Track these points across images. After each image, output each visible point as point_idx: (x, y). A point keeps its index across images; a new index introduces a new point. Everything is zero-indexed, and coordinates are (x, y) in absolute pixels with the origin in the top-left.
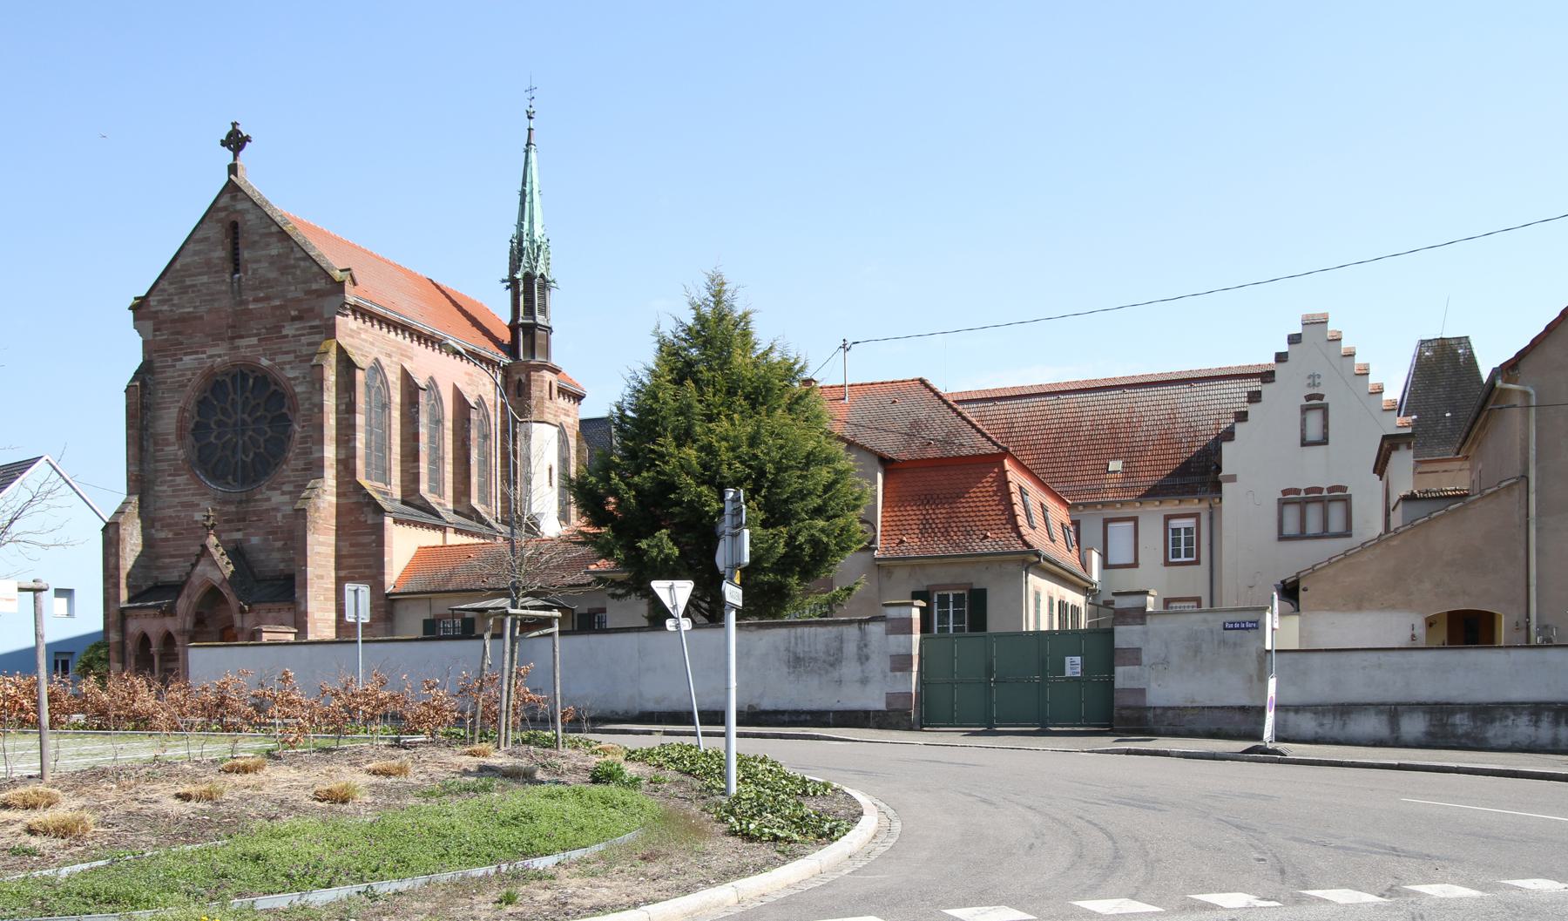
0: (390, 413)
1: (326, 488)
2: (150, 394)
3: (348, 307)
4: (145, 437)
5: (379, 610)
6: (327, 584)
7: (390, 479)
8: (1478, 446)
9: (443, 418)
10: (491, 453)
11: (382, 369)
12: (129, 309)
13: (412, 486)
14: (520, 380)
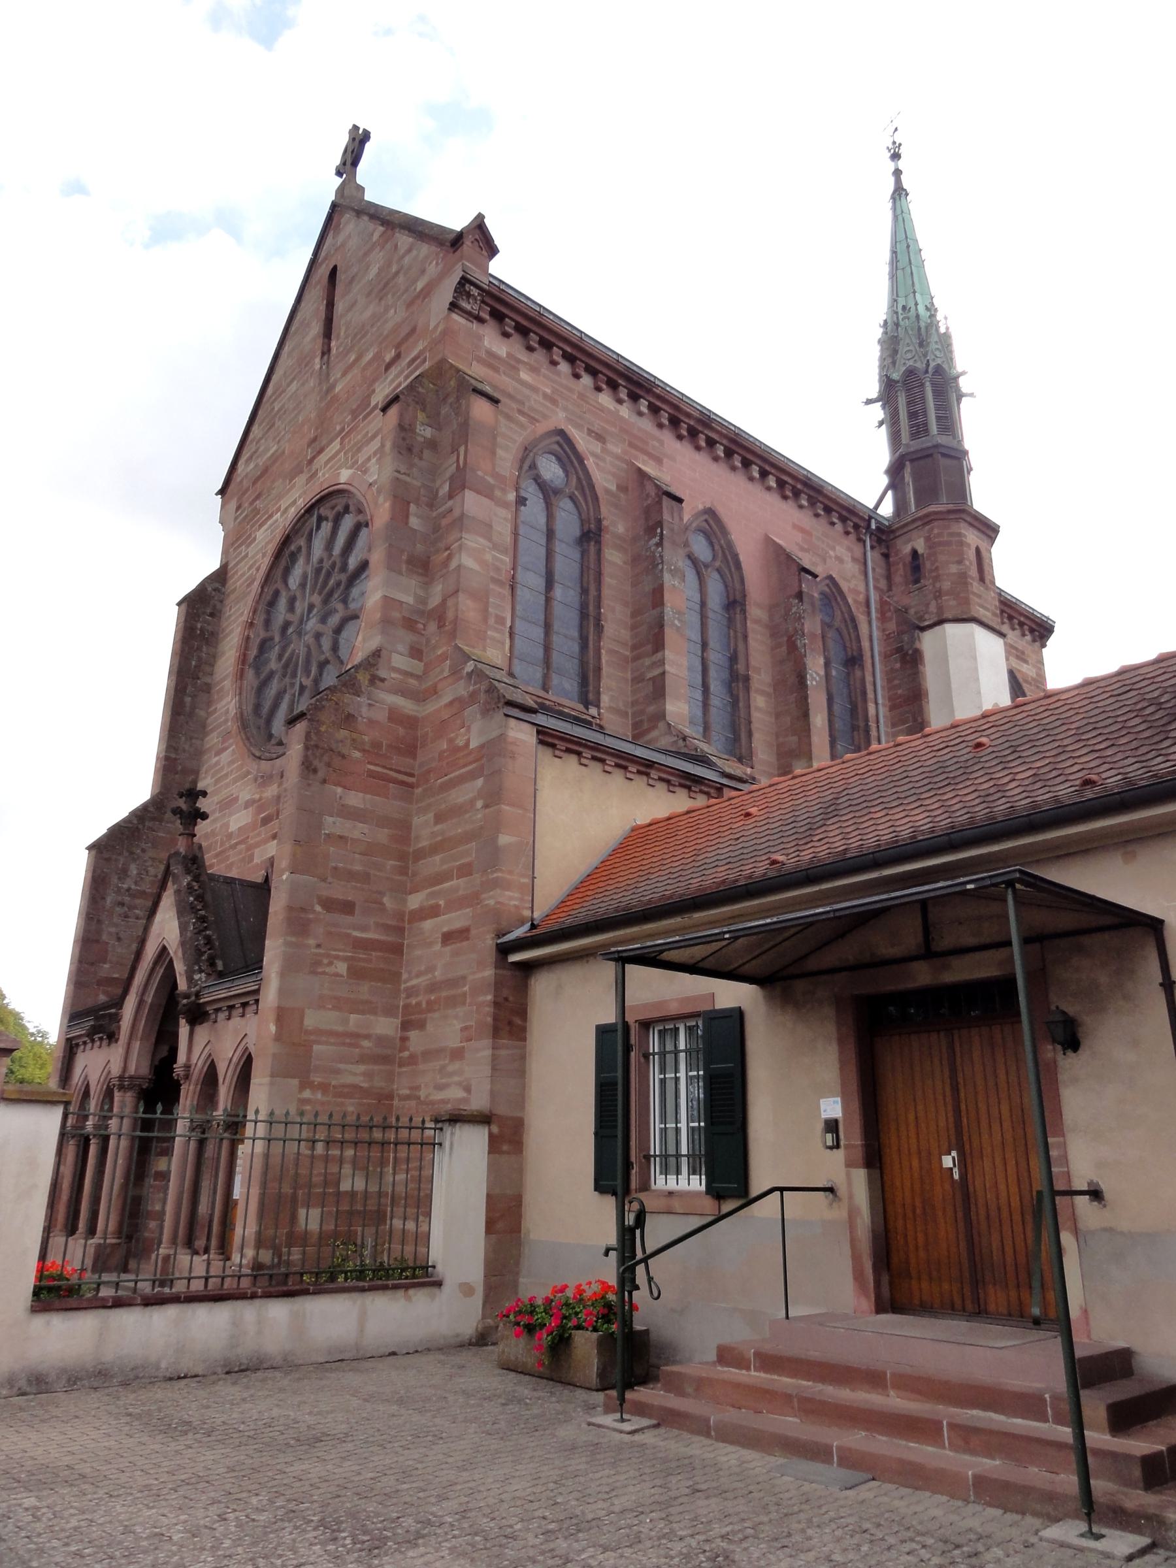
0: (599, 552)
1: (382, 673)
2: (212, 615)
3: (475, 292)
4: (190, 689)
5: (481, 999)
6: (364, 929)
7: (599, 693)
8: (450, 1154)
9: (745, 596)
10: (864, 693)
11: (581, 460)
12: (217, 494)
13: (651, 709)
14: (915, 553)
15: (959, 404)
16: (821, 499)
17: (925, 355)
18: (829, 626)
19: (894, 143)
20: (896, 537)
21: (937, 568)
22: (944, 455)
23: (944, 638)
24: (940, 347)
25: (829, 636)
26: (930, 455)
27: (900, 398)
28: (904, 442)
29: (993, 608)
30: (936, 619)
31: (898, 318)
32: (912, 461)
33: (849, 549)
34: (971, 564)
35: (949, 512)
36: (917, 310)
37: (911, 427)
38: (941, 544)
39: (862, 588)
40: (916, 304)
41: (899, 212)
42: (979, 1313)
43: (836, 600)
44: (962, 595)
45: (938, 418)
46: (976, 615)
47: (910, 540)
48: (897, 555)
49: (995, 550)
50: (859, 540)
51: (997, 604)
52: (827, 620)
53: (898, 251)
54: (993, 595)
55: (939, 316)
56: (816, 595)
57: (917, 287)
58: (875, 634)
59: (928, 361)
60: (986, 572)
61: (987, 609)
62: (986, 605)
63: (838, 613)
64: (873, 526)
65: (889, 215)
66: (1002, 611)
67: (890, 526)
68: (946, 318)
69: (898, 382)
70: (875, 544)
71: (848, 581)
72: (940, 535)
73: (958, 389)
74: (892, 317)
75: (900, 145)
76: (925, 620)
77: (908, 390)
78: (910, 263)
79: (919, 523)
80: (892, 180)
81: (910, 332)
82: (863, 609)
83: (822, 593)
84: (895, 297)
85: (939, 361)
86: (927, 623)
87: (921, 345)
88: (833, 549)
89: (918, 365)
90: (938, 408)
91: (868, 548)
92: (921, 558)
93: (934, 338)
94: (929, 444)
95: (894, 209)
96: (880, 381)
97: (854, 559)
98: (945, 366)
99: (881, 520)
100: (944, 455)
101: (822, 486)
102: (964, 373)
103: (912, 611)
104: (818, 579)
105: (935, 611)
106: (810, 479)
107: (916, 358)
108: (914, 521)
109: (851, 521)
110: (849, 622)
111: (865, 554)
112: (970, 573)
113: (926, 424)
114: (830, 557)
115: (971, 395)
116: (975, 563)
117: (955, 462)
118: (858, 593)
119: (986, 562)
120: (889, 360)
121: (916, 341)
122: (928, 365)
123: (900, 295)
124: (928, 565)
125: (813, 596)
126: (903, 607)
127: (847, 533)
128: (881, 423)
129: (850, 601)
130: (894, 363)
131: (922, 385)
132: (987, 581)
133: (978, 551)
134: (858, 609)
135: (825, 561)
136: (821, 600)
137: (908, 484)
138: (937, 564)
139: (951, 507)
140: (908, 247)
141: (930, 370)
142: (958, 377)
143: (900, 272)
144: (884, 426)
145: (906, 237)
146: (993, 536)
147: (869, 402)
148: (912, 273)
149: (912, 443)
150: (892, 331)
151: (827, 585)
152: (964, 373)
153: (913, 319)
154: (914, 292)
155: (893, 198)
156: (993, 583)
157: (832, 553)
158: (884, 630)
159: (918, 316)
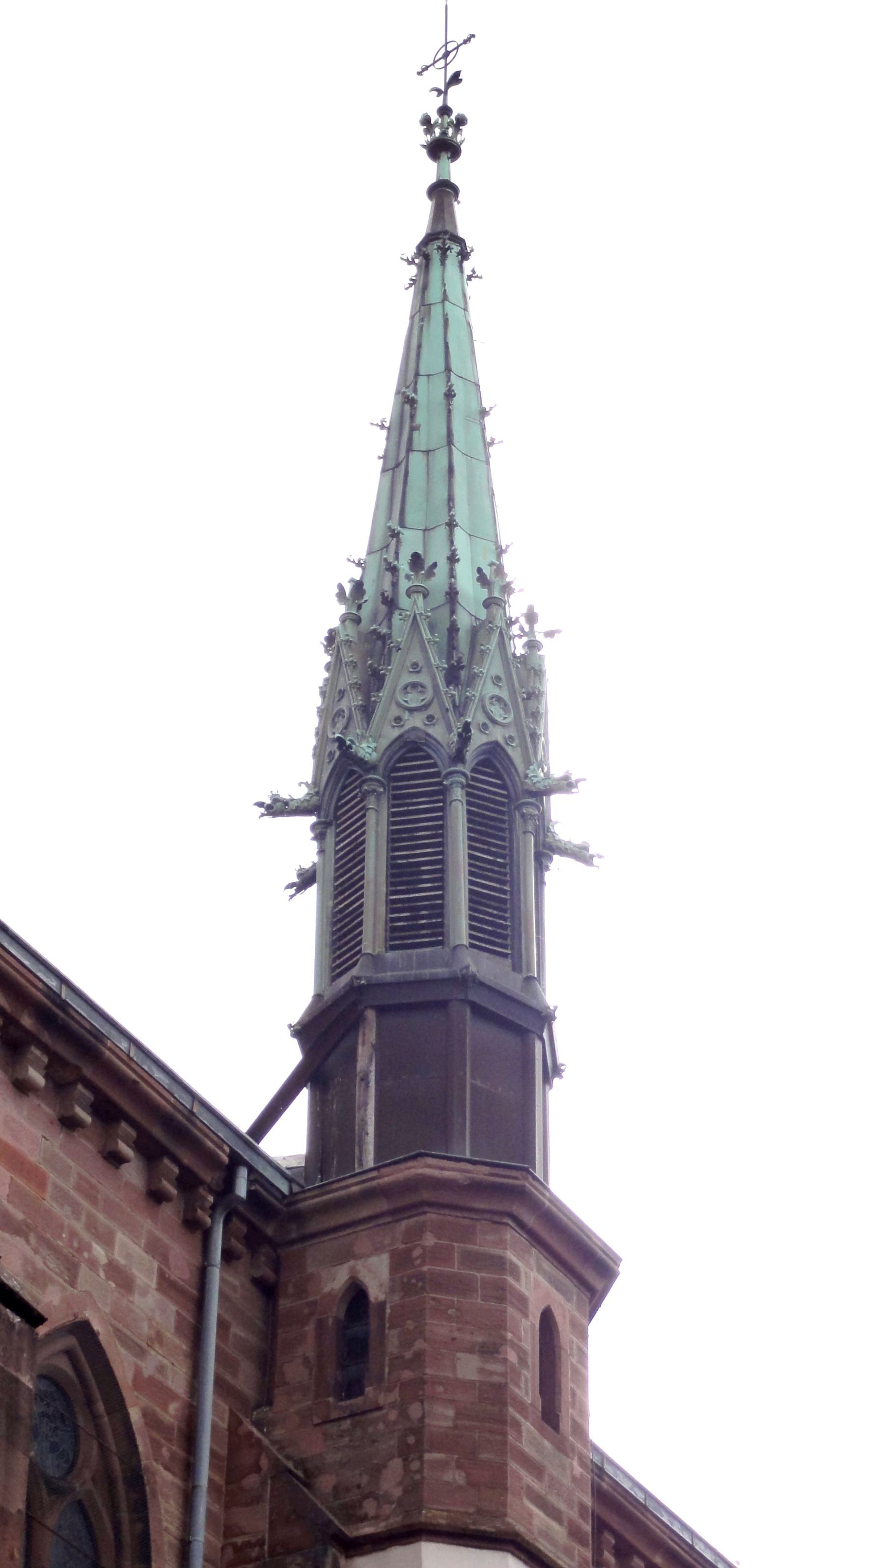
15: (541, 868)
16: (87, 1071)
17: (460, 709)
18: (56, 1491)
19: (445, 111)
20: (304, 1238)
21: (419, 1358)
22: (479, 1011)
23: (420, 1551)
24: (505, 695)
25: (51, 1521)
26: (442, 1005)
27: (371, 818)
28: (367, 947)
29: (574, 1514)
30: (395, 1521)
31: (395, 585)
32: (381, 1010)
33: (154, 1248)
34: (523, 1360)
35: (477, 1187)
36: (452, 574)
37: (393, 907)
38: (441, 1283)
39: (178, 1381)
40: (453, 559)
41: (434, 295)
42: (489, 632)
43: (90, 1403)
44: (484, 1456)
45: (475, 898)
46: (520, 1528)
47: (347, 1255)
48: (301, 1292)
49: (598, 1328)
50: (191, 1224)
51: (588, 1501)
52: (52, 1467)
53: (421, 397)
54: (578, 1470)
55: (516, 607)
56: (26, 1380)
57: (461, 513)
58: (201, 1535)
59: (467, 727)
60: (566, 1397)
61: (554, 1514)
62: (552, 1499)
63: (90, 1451)
64: (242, 1189)
65: (407, 299)
66: (600, 1526)
67: (291, 1199)
68: (531, 617)
69: (373, 768)
70: (239, 1247)
71: (140, 1352)
72: (440, 1255)
73: (542, 827)
74: (380, 578)
75: (461, 121)
76: (364, 1518)
77: (397, 799)
78: (450, 442)
79: (383, 1205)
80: (426, 206)
81: (426, 635)
82: (171, 1449)
83: (47, 1377)
84: (394, 524)
85: (497, 734)
86: (367, 1529)
87: (453, 676)
88: (108, 1241)
89: (437, 732)
90: (476, 870)
91: (217, 1255)
92: (372, 1313)
93: (492, 666)
94: (441, 971)
95: (421, 285)
96: (319, 753)
97: (166, 1284)
98: (515, 754)
99: (269, 1173)
100: (479, 1011)
101: (99, 1037)
102: (567, 785)
103: (326, 1483)
104: (42, 1330)
105: (397, 1492)
106: (64, 1006)
107: (434, 710)
108: (369, 1195)
109: (176, 1160)
110: (121, 1487)
111: (203, 1274)
112: (520, 1393)
113: (438, 910)
114: (93, 1263)
115: (581, 854)
116: (534, 1359)
117: (508, 1040)
118: (165, 1394)
119: (567, 1361)
120: (354, 700)
121: (437, 661)
122: (465, 737)
123: (409, 519)
124: (393, 1342)
125: (17, 1381)
126: (300, 1463)
127: (156, 1197)
128: (306, 880)
129: (135, 1415)
130: (367, 711)
131: (443, 792)
132: (566, 1426)
133: (547, 1319)
134: (156, 1445)
135: (71, 1270)
136: (40, 1396)
137: (365, 1079)
138: (419, 1345)
139: (481, 1173)
140: (449, 395)
141: (470, 754)
142: (548, 792)
143: (417, 460)
144: (313, 891)
145: (448, 369)
146: (599, 1285)
147: (300, 866)
148: (451, 470)
149: (390, 955)
150: (374, 619)
151: (69, 1353)
152: (567, 785)
153: (439, 597)
154: (451, 525)
155: (423, 253)
156: (580, 1431)
157: (99, 1251)
158: (229, 1531)
159: (452, 595)
